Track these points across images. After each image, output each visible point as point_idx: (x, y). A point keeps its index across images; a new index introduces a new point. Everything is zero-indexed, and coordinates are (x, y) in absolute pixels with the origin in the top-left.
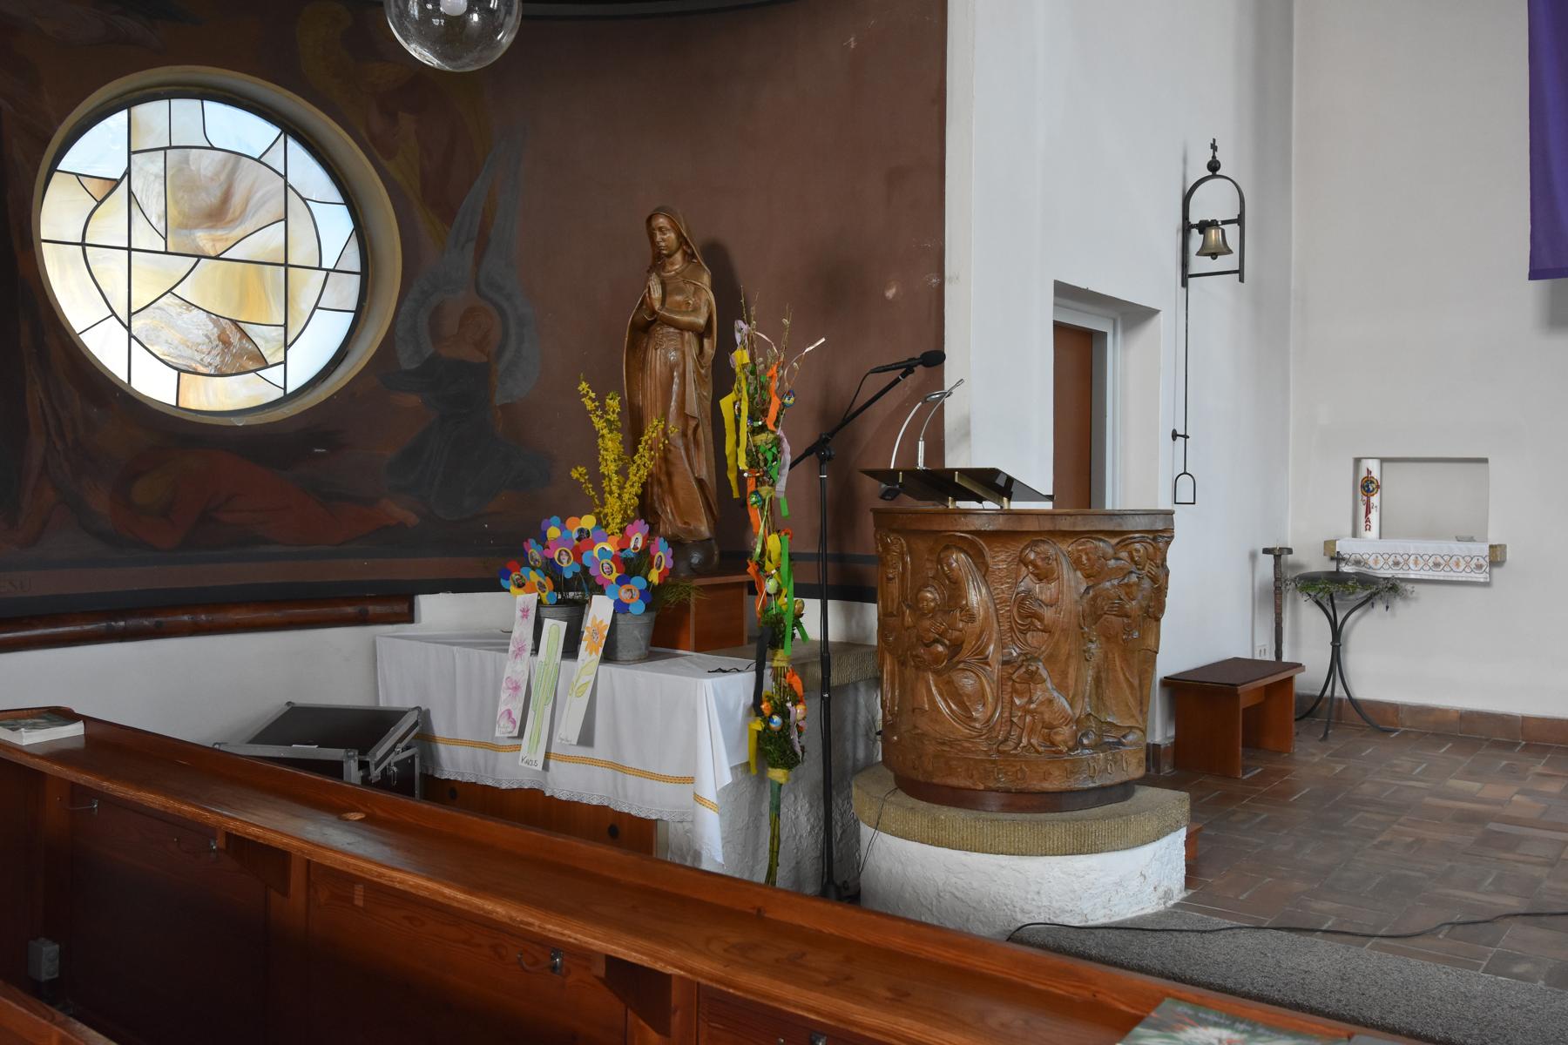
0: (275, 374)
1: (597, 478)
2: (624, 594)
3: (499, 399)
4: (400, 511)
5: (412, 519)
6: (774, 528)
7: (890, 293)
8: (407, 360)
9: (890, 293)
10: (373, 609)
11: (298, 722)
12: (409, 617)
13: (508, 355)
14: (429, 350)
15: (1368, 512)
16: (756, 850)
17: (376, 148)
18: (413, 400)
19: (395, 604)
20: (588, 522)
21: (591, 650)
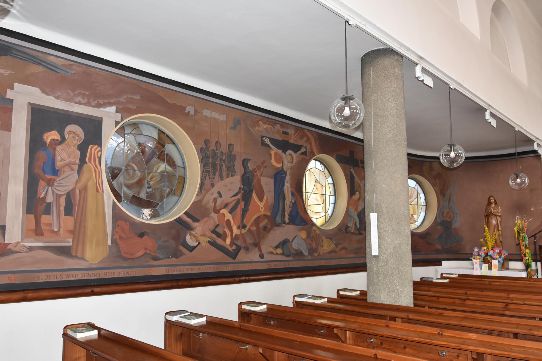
0: (416, 223)
1: (485, 241)
2: (500, 259)
3: (453, 227)
4: (438, 247)
5: (440, 248)
6: (526, 248)
7: (532, 209)
8: (439, 221)
9: (532, 209)
10: (30, 295)
11: (341, 298)
12: (441, 265)
13: (455, 219)
14: (442, 219)
15: (525, 304)
16: (454, 343)
17: (434, 185)
18: (440, 227)
19: (438, 263)
20: (485, 248)
21: (495, 268)
